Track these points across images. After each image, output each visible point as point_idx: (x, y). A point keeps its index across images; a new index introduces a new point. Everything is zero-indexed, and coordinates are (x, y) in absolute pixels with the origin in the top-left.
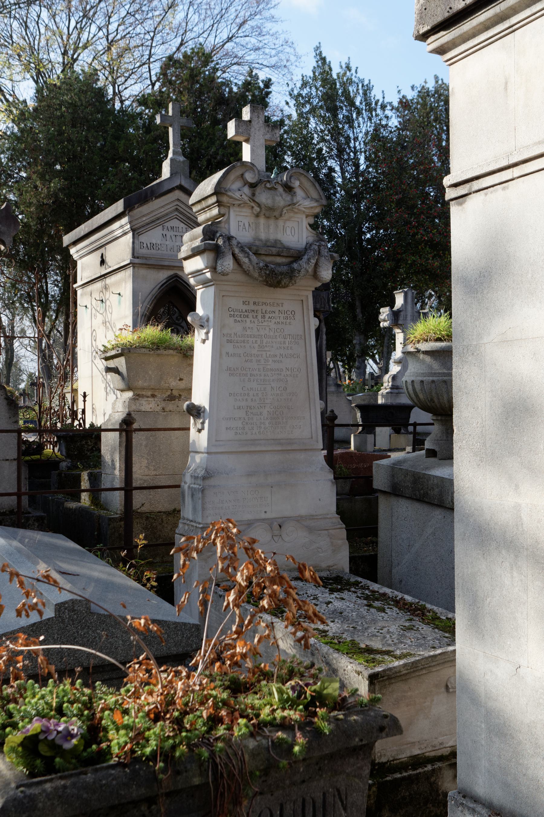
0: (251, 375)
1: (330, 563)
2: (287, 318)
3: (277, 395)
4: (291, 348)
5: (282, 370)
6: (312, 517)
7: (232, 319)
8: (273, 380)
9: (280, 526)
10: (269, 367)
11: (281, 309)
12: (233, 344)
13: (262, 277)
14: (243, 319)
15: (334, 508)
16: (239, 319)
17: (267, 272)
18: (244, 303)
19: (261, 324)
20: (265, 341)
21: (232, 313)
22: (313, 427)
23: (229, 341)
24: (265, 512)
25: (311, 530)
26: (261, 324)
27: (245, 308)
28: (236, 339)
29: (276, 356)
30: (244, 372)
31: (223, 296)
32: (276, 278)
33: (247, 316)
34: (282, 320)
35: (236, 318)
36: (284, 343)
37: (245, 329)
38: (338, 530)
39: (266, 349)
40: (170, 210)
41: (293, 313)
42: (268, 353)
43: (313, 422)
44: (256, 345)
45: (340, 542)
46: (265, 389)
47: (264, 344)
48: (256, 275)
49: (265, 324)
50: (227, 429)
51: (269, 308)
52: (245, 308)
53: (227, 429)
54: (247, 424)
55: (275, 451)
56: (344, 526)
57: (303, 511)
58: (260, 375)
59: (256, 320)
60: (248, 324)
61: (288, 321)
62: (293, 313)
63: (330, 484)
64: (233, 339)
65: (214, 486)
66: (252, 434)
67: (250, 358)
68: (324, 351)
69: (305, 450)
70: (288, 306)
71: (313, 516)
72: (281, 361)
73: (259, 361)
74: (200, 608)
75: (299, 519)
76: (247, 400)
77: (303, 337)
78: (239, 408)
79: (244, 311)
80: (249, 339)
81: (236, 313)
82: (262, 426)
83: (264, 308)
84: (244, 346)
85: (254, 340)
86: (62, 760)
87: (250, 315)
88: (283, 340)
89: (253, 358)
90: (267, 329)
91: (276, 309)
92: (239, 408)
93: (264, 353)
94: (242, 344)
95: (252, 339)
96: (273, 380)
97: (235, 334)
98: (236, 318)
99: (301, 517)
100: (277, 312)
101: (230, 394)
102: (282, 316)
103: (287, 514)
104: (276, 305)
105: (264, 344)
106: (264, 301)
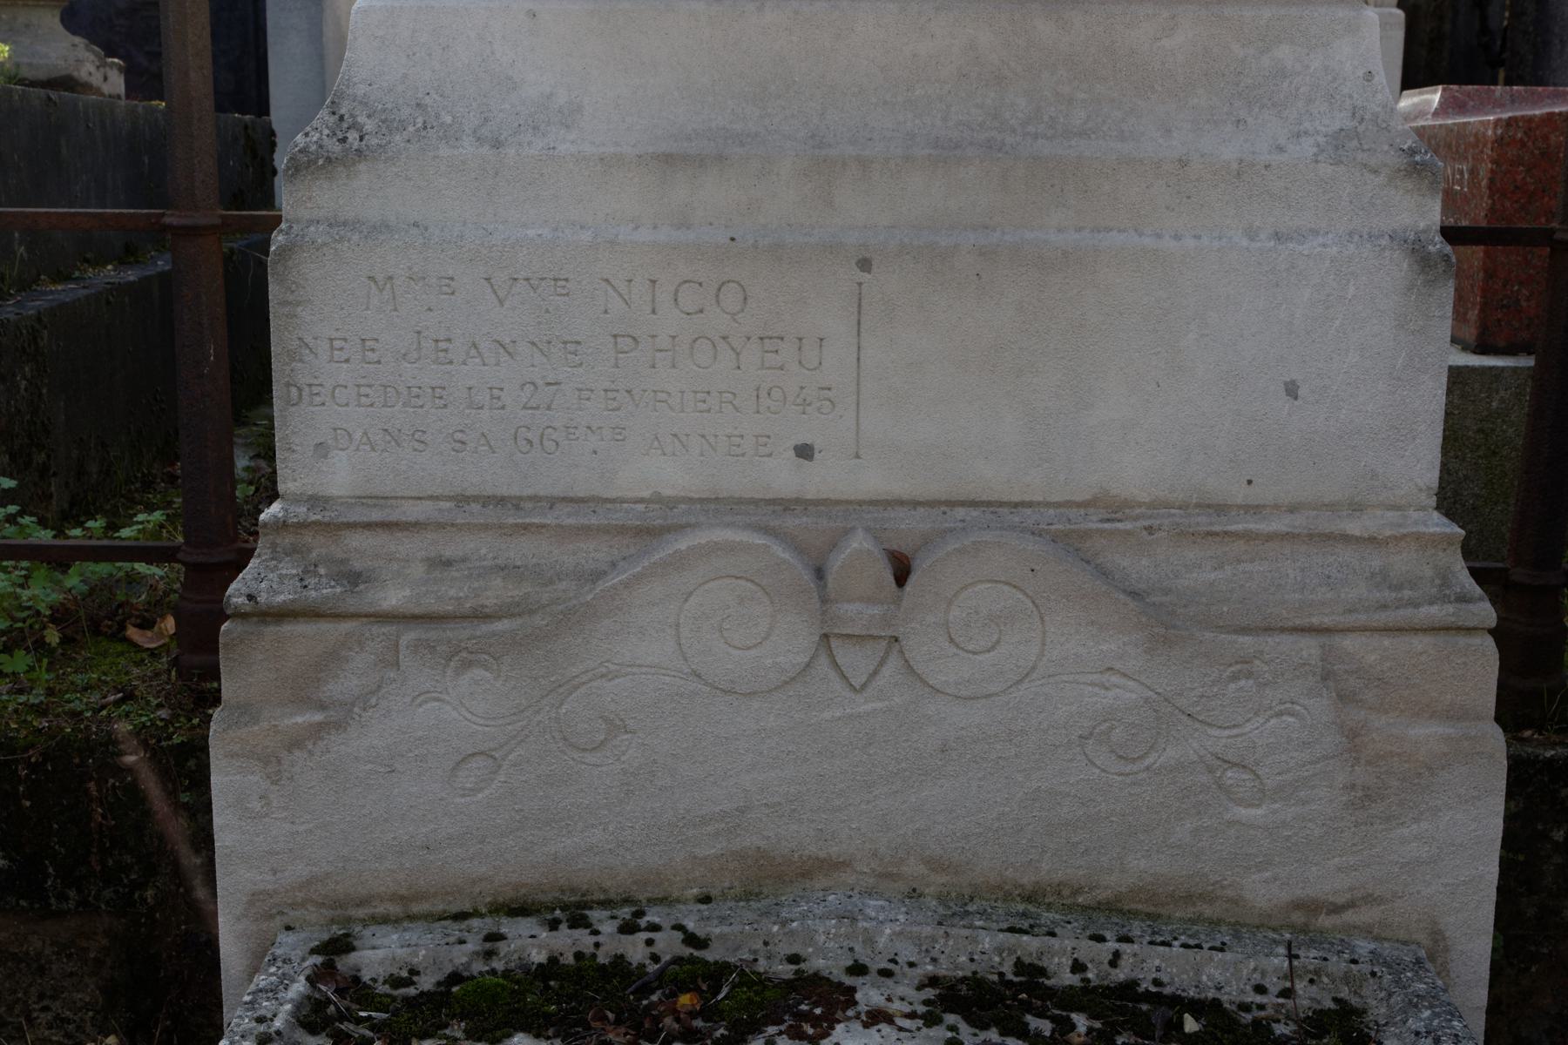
1: (1324, 878)
6: (1206, 521)
9: (902, 572)
15: (1420, 463)
24: (804, 452)
25: (1163, 618)
38: (1419, 643)
45: (1426, 733)
56: (1485, 612)
57: (1134, 467)
63: (1397, 268)
71: (1221, 509)
74: (457, 1030)
75: (1081, 541)
86: (237, 452)
99: (1114, 508)
103: (992, 476)
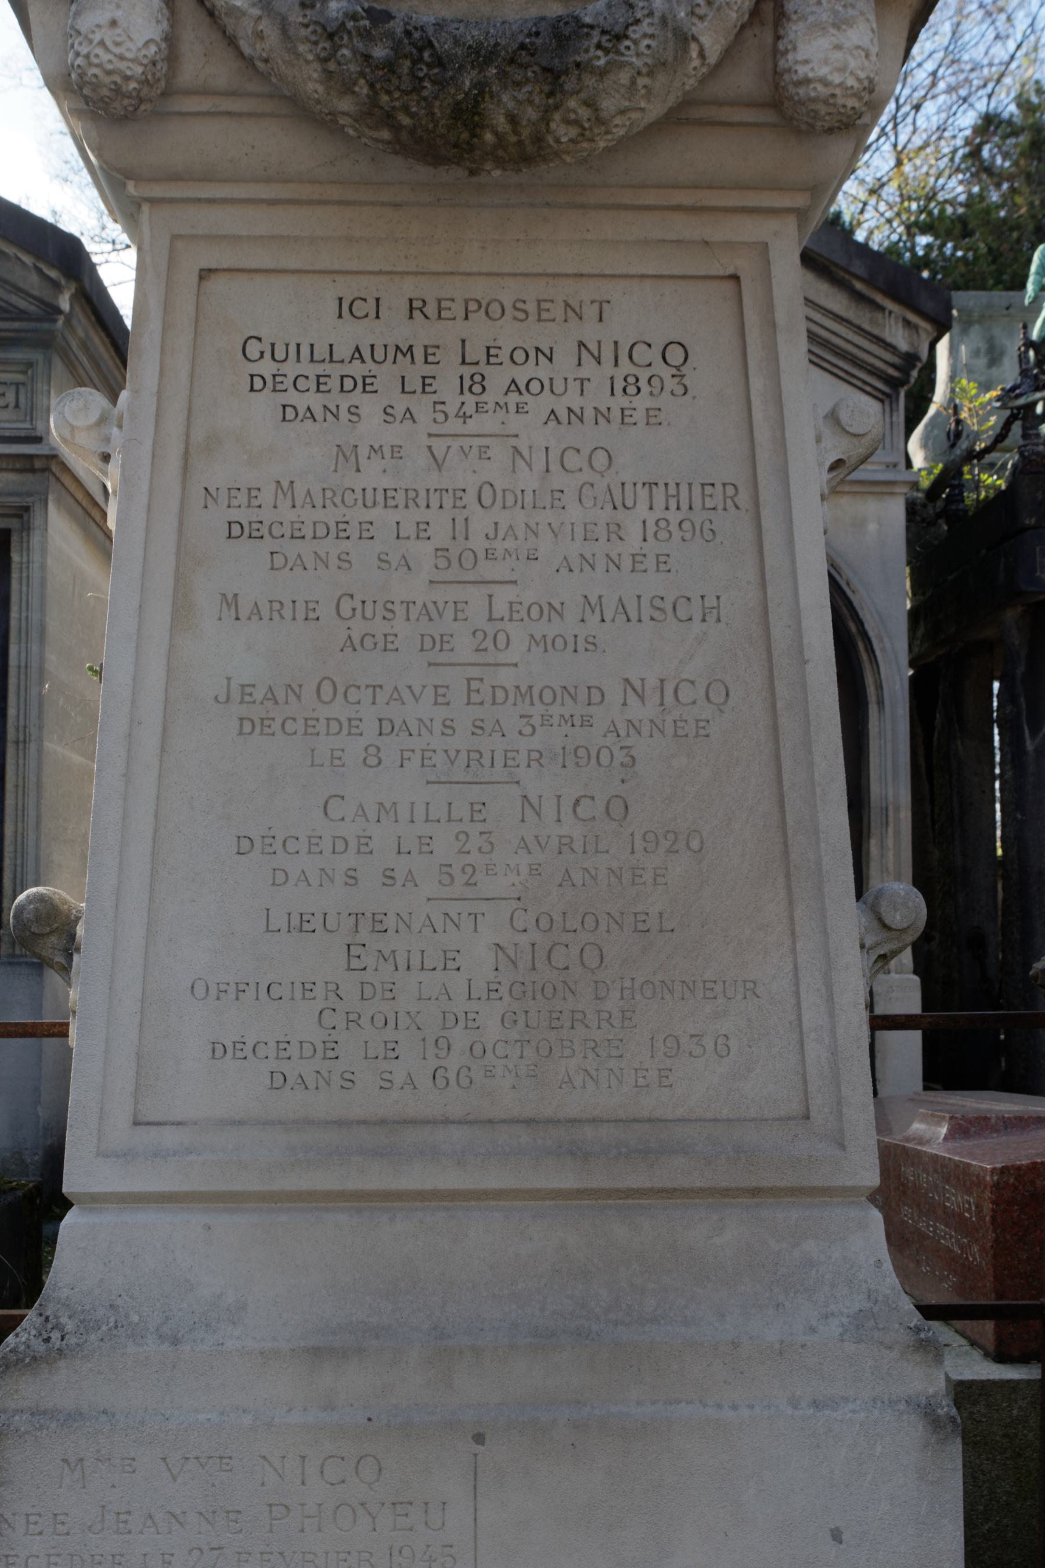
0: (386, 727)
2: (632, 386)
3: (565, 845)
4: (661, 561)
5: (596, 694)
7: (265, 403)
8: (537, 759)
10: (506, 677)
11: (590, 332)
12: (268, 544)
13: (348, 89)
14: (334, 399)
16: (315, 400)
17: (380, 52)
18: (345, 308)
19: (454, 425)
20: (481, 522)
21: (267, 368)
22: (816, 1051)
23: (235, 531)
26: (454, 425)
27: (348, 335)
28: (289, 515)
29: (557, 611)
30: (339, 710)
31: (205, 274)
32: (440, 84)
33: (366, 384)
34: (598, 396)
35: (292, 397)
36: (616, 532)
37: (346, 455)
39: (488, 570)
40: (879, 364)
41: (675, 355)
42: (503, 596)
43: (813, 1016)
44: (423, 551)
46: (477, 809)
47: (478, 543)
48: (311, 82)
49: (487, 422)
50: (217, 1050)
51: (508, 335)
52: (348, 335)
53: (217, 1050)
54: (352, 1021)
55: (534, 1194)
58: (448, 727)
59: (422, 406)
60: (371, 426)
61: (643, 402)
62: (675, 355)
64: (267, 515)
65: (72, 1418)
66: (387, 1085)
67: (379, 627)
68: (155, 324)
69: (756, 1192)
70: (638, 316)
72: (592, 643)
73: (442, 642)
76: (352, 878)
77: (744, 498)
78: (302, 925)
79: (343, 351)
80: (376, 514)
81: (291, 369)
82: (459, 1037)
83: (480, 332)
84: (344, 559)
85: (409, 518)
87: (386, 375)
88: (606, 514)
89: (399, 625)
90: (499, 452)
91: (562, 340)
92: (302, 925)
93: (476, 596)
94: (330, 547)
95: (393, 516)
96: (537, 759)
97: (284, 489)
98: (292, 397)
100: (565, 357)
101: (244, 846)
102: (598, 375)
104: (558, 311)
105: (478, 543)
106: (480, 289)
